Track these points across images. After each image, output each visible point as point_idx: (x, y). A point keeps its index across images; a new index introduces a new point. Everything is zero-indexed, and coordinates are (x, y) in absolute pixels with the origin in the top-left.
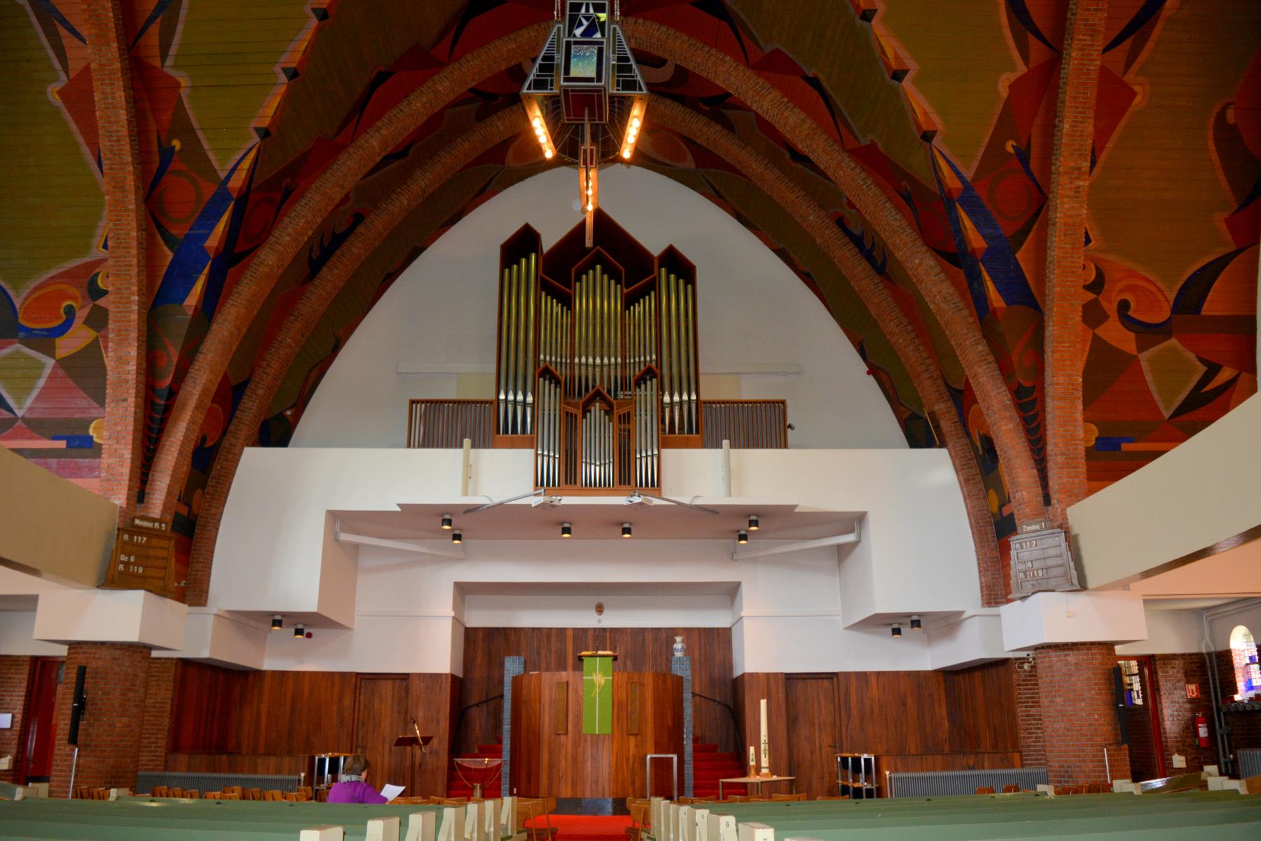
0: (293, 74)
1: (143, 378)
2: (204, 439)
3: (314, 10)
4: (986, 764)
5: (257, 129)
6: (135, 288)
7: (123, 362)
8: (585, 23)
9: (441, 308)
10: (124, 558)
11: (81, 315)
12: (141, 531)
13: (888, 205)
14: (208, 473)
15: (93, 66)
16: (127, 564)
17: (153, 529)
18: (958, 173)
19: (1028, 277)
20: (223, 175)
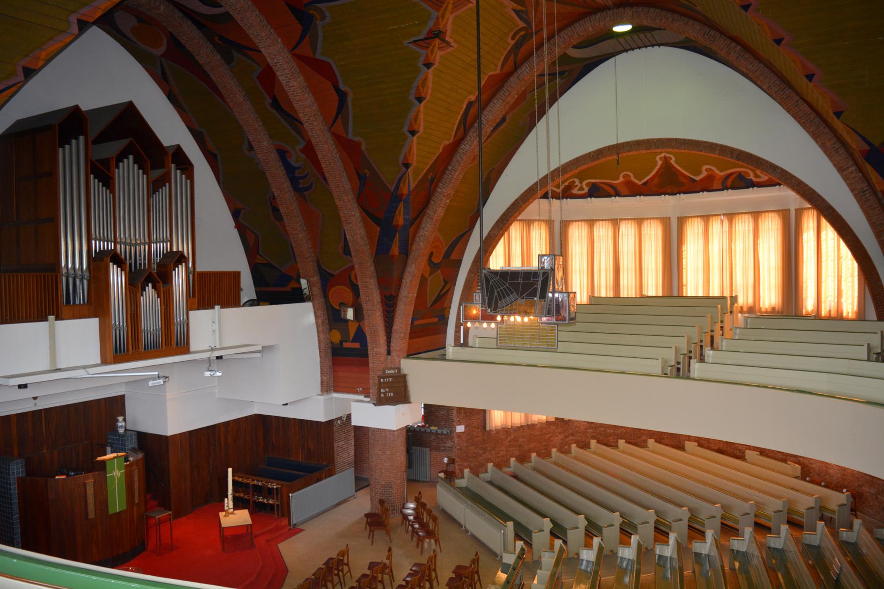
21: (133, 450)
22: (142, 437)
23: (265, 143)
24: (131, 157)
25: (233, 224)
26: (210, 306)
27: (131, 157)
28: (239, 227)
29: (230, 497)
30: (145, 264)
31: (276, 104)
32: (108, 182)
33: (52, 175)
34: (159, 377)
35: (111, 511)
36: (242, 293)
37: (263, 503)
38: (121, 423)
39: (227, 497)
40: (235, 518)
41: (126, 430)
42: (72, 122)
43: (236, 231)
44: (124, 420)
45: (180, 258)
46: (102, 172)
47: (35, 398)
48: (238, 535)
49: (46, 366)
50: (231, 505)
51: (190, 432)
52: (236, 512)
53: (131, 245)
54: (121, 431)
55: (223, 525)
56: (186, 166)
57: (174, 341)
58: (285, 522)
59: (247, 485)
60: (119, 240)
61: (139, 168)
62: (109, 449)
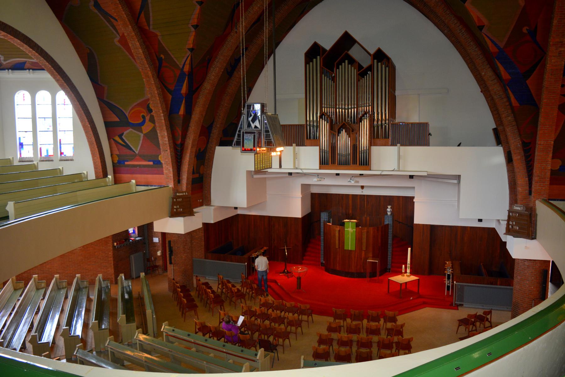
0: (196, 27)
1: (171, 141)
2: (200, 150)
3: (197, 2)
4: (498, 283)
5: (188, 49)
6: (161, 111)
7: (164, 137)
8: (253, 115)
9: (281, 86)
10: (175, 207)
11: (147, 118)
12: (179, 197)
13: (472, 43)
14: (204, 160)
15: (126, 34)
16: (177, 209)
17: (184, 195)
18: (496, 45)
19: (532, 91)
20: (181, 67)
24: (346, 61)
27: (346, 61)
39: (406, 264)
43: (482, 94)
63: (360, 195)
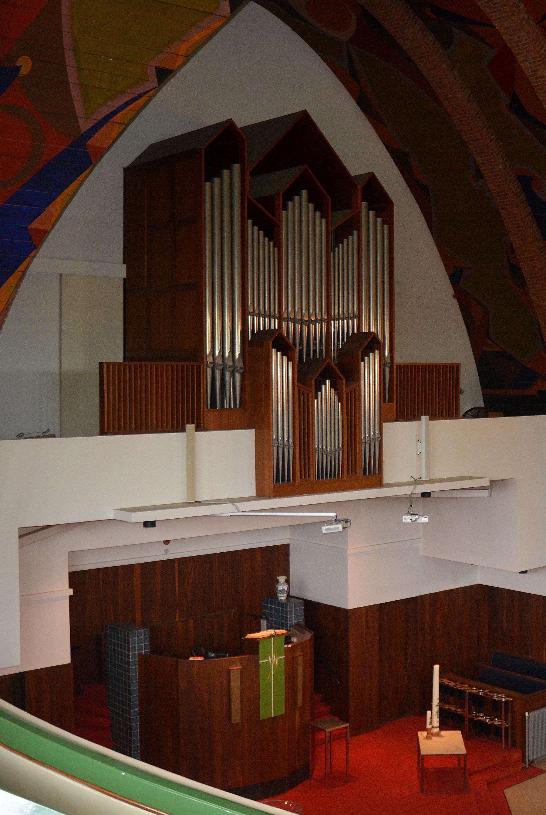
20: (85, 125)
21: (298, 626)
22: (312, 609)
23: (500, 167)
24: (304, 193)
25: (451, 292)
26: (414, 416)
27: (304, 193)
28: (461, 296)
29: (435, 709)
30: (321, 351)
31: (516, 106)
32: (272, 231)
33: (194, 222)
34: (337, 521)
35: (263, 716)
36: (462, 397)
37: (484, 723)
38: (282, 587)
39: (431, 709)
40: (442, 742)
41: (289, 596)
42: (222, 145)
43: (455, 302)
44: (287, 581)
45: (371, 343)
46: (264, 216)
47: (167, 542)
48: (442, 774)
49: (179, 497)
50: (436, 722)
51: (381, 606)
52: (443, 733)
53: (302, 322)
54: (282, 597)
55: (423, 752)
56: (382, 205)
57: (360, 467)
58: (516, 755)
59: (462, 693)
60: (285, 316)
61: (316, 209)
62: (264, 623)
63: (164, 562)
